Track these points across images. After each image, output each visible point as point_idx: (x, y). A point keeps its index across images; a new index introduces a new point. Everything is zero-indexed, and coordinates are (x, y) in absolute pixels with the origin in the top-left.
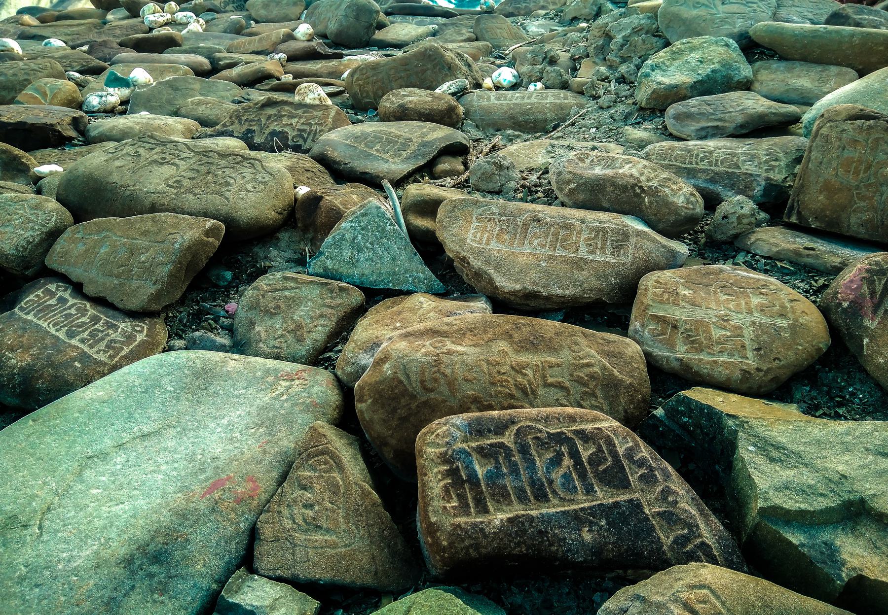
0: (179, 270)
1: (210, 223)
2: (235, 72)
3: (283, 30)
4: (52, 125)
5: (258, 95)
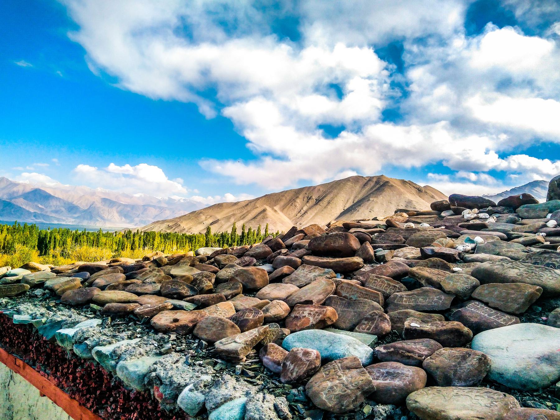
0: (526, 301)
1: (538, 287)
2: (521, 239)
3: (541, 222)
4: (453, 254)
5: (534, 250)
